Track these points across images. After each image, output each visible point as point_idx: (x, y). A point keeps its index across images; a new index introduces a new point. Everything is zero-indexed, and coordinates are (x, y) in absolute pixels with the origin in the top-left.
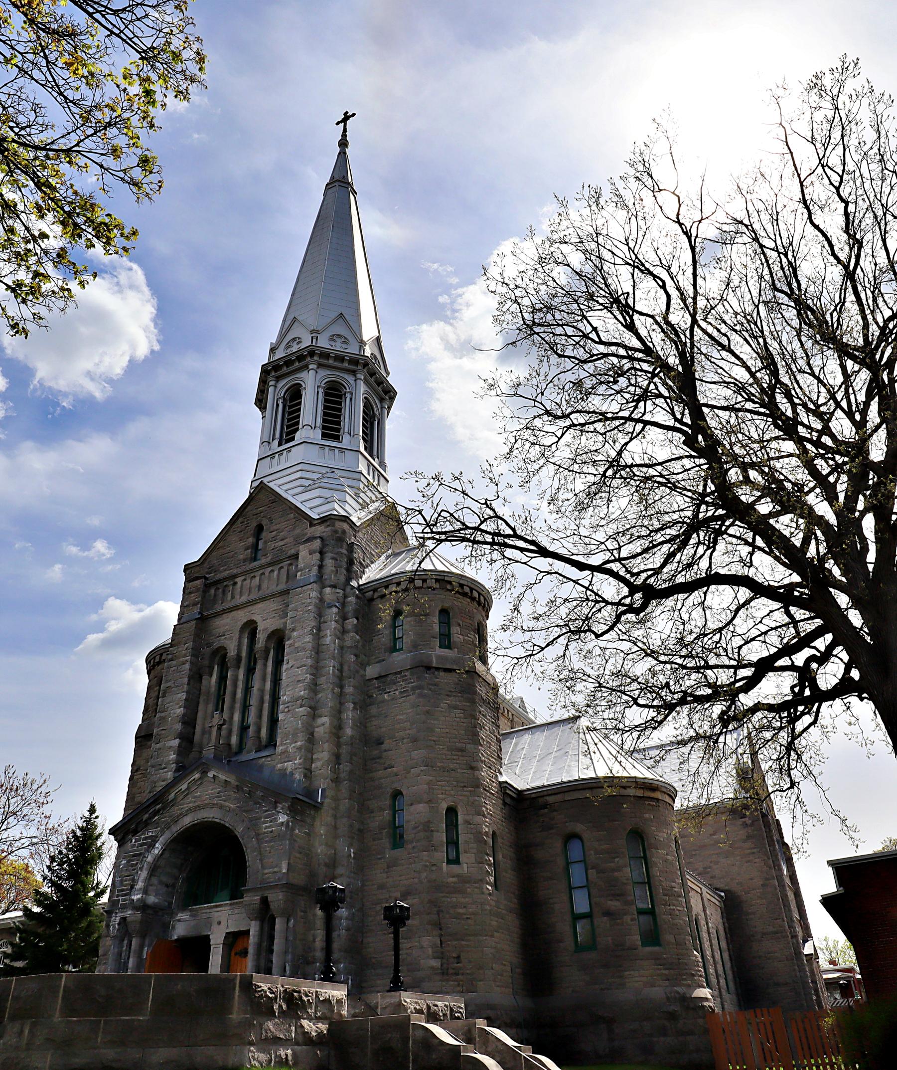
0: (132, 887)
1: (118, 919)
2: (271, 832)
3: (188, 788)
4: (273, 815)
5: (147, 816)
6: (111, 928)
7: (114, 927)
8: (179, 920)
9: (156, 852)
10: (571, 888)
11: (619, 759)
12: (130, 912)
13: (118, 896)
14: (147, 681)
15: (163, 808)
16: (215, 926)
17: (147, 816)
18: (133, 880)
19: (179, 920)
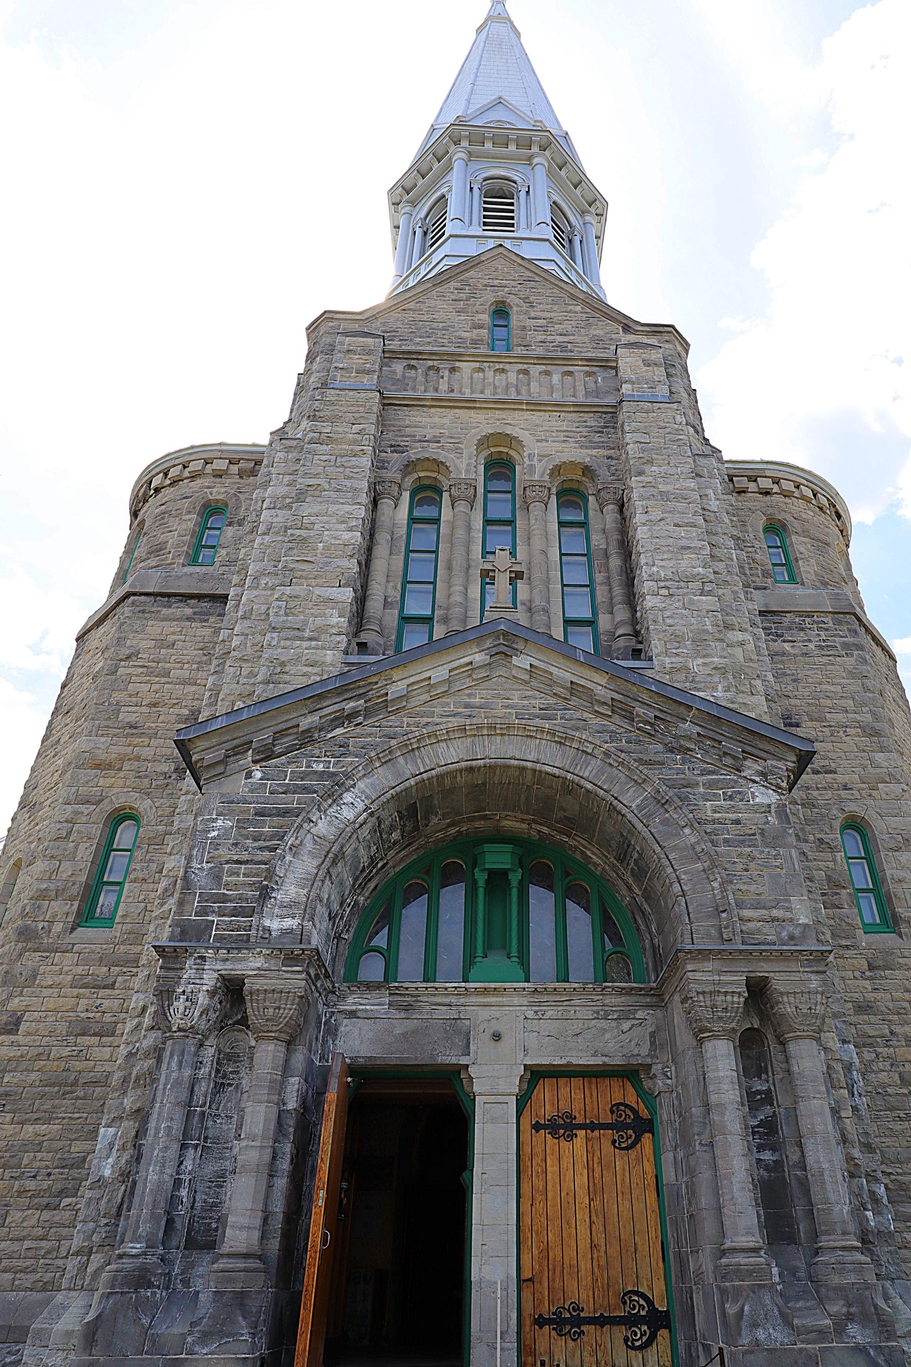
0: (265, 894)
1: (209, 979)
2: (737, 822)
3: (449, 681)
4: (734, 784)
5: (314, 719)
6: (180, 1004)
7: (191, 1000)
8: (352, 1014)
9: (348, 814)
10: (101, 1036)
11: (313, 584)
12: (259, 962)
13: (203, 912)
14: (855, 575)
15: (368, 713)
16: (480, 1046)
17: (314, 719)
18: (270, 874)
19: (352, 1014)
